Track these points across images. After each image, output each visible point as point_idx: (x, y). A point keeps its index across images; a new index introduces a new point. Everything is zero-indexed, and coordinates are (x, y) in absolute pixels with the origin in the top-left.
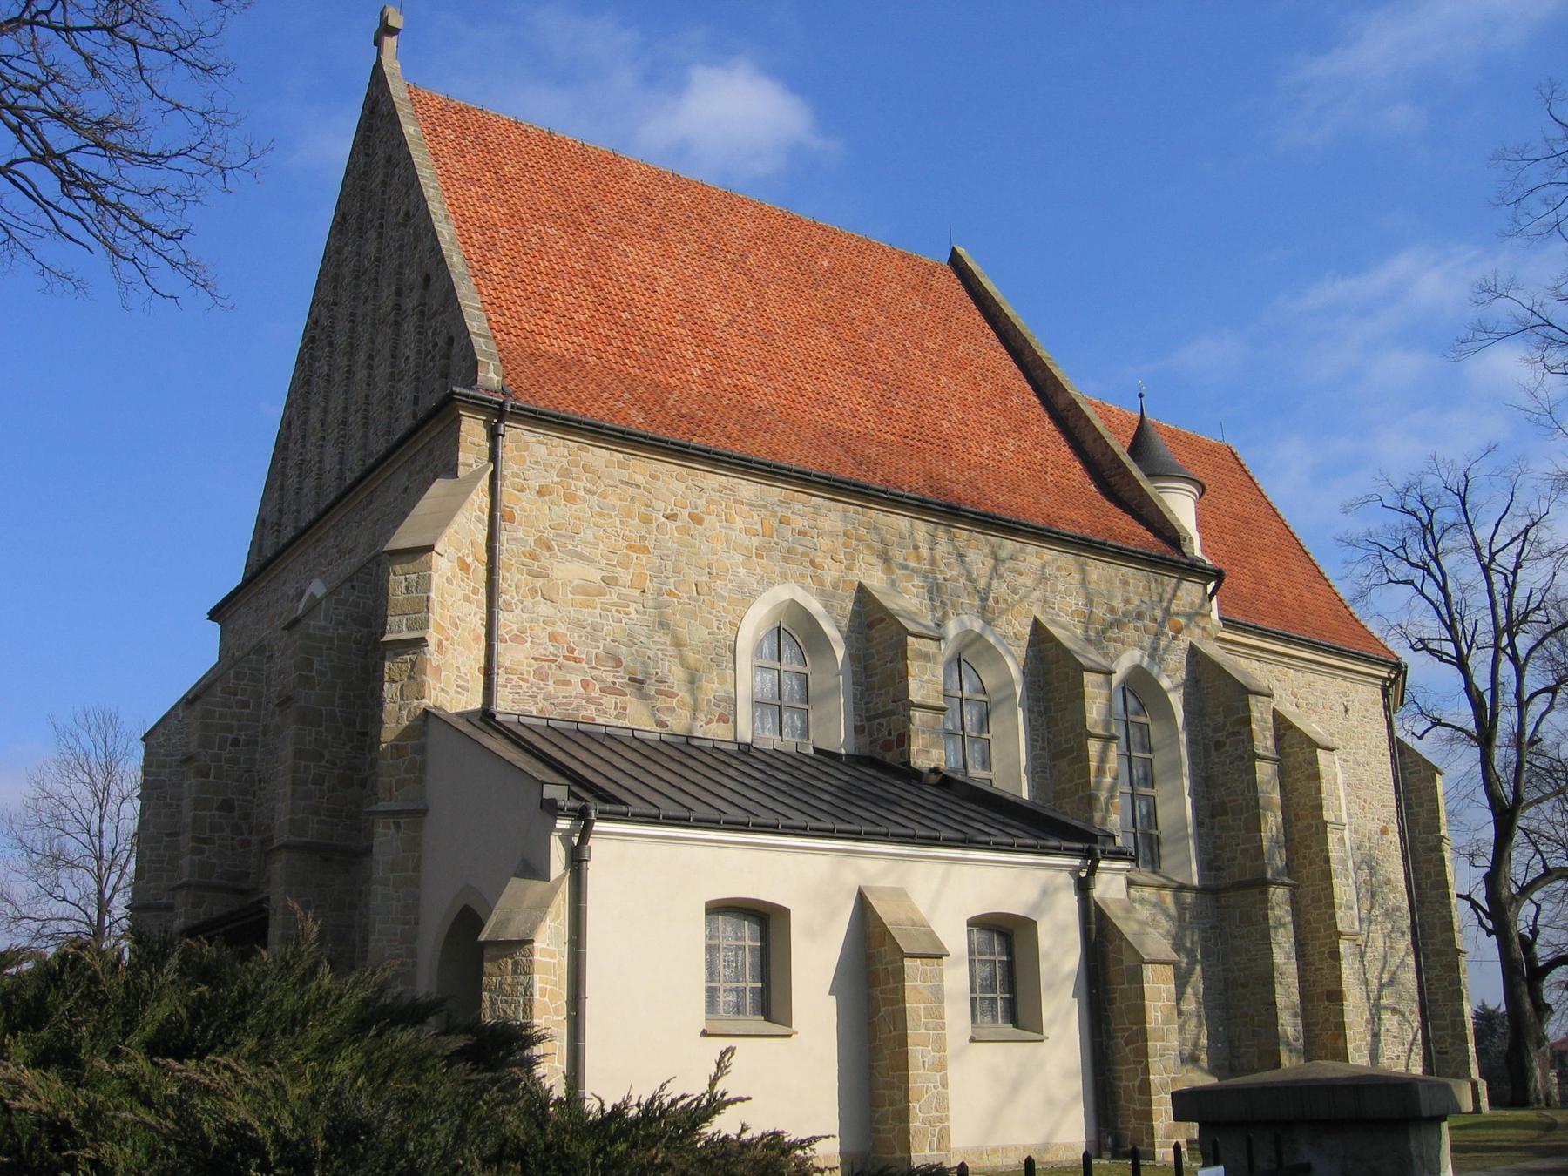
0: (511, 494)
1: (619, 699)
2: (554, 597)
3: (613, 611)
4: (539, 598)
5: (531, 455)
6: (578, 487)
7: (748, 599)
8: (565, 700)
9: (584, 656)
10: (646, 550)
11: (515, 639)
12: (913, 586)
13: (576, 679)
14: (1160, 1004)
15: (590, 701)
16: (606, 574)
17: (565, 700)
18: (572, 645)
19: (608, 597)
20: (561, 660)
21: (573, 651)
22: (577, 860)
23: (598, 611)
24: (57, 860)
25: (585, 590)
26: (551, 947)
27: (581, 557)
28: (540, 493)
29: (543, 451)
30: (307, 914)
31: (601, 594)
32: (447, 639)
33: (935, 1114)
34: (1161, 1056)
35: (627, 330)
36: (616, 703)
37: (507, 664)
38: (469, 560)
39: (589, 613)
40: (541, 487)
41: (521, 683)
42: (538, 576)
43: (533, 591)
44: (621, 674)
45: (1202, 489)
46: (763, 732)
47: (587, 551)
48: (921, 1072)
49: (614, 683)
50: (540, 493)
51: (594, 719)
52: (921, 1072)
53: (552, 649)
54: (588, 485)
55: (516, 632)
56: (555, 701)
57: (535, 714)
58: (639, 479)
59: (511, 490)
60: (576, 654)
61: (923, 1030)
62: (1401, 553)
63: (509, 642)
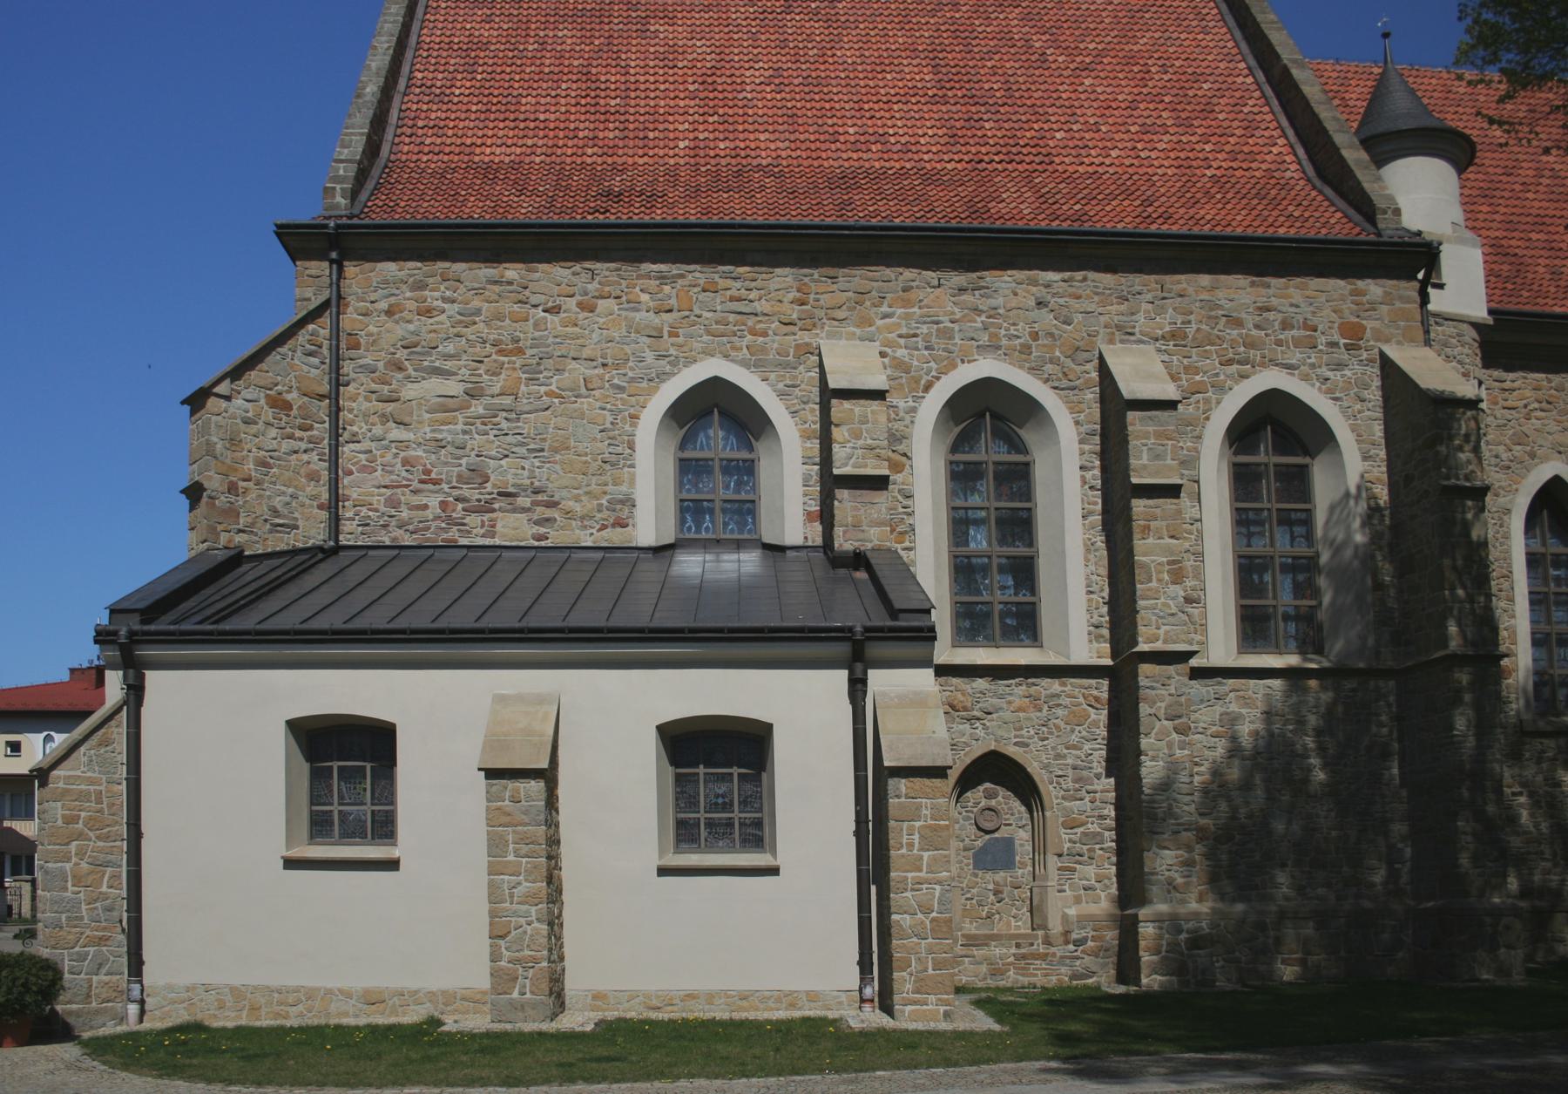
0: (354, 320)
2: (407, 419)
3: (478, 425)
4: (391, 424)
7: (662, 377)
8: (421, 525)
9: (443, 477)
10: (520, 351)
12: (900, 336)
13: (434, 502)
14: (917, 824)
15: (452, 522)
16: (470, 386)
17: (421, 525)
18: (429, 466)
19: (473, 409)
20: (415, 484)
22: (136, 692)
25: (446, 407)
26: (89, 774)
28: (389, 313)
32: (248, 480)
33: (527, 952)
34: (912, 890)
36: (482, 521)
38: (291, 397)
39: (448, 431)
40: (390, 306)
41: (371, 513)
44: (489, 489)
47: (448, 365)
48: (508, 904)
49: (479, 500)
50: (389, 313)
51: (456, 541)
52: (508, 904)
53: (404, 474)
54: (448, 293)
55: (364, 462)
56: (411, 528)
57: (388, 543)
59: (355, 316)
60: (433, 476)
61: (511, 858)
63: (356, 474)
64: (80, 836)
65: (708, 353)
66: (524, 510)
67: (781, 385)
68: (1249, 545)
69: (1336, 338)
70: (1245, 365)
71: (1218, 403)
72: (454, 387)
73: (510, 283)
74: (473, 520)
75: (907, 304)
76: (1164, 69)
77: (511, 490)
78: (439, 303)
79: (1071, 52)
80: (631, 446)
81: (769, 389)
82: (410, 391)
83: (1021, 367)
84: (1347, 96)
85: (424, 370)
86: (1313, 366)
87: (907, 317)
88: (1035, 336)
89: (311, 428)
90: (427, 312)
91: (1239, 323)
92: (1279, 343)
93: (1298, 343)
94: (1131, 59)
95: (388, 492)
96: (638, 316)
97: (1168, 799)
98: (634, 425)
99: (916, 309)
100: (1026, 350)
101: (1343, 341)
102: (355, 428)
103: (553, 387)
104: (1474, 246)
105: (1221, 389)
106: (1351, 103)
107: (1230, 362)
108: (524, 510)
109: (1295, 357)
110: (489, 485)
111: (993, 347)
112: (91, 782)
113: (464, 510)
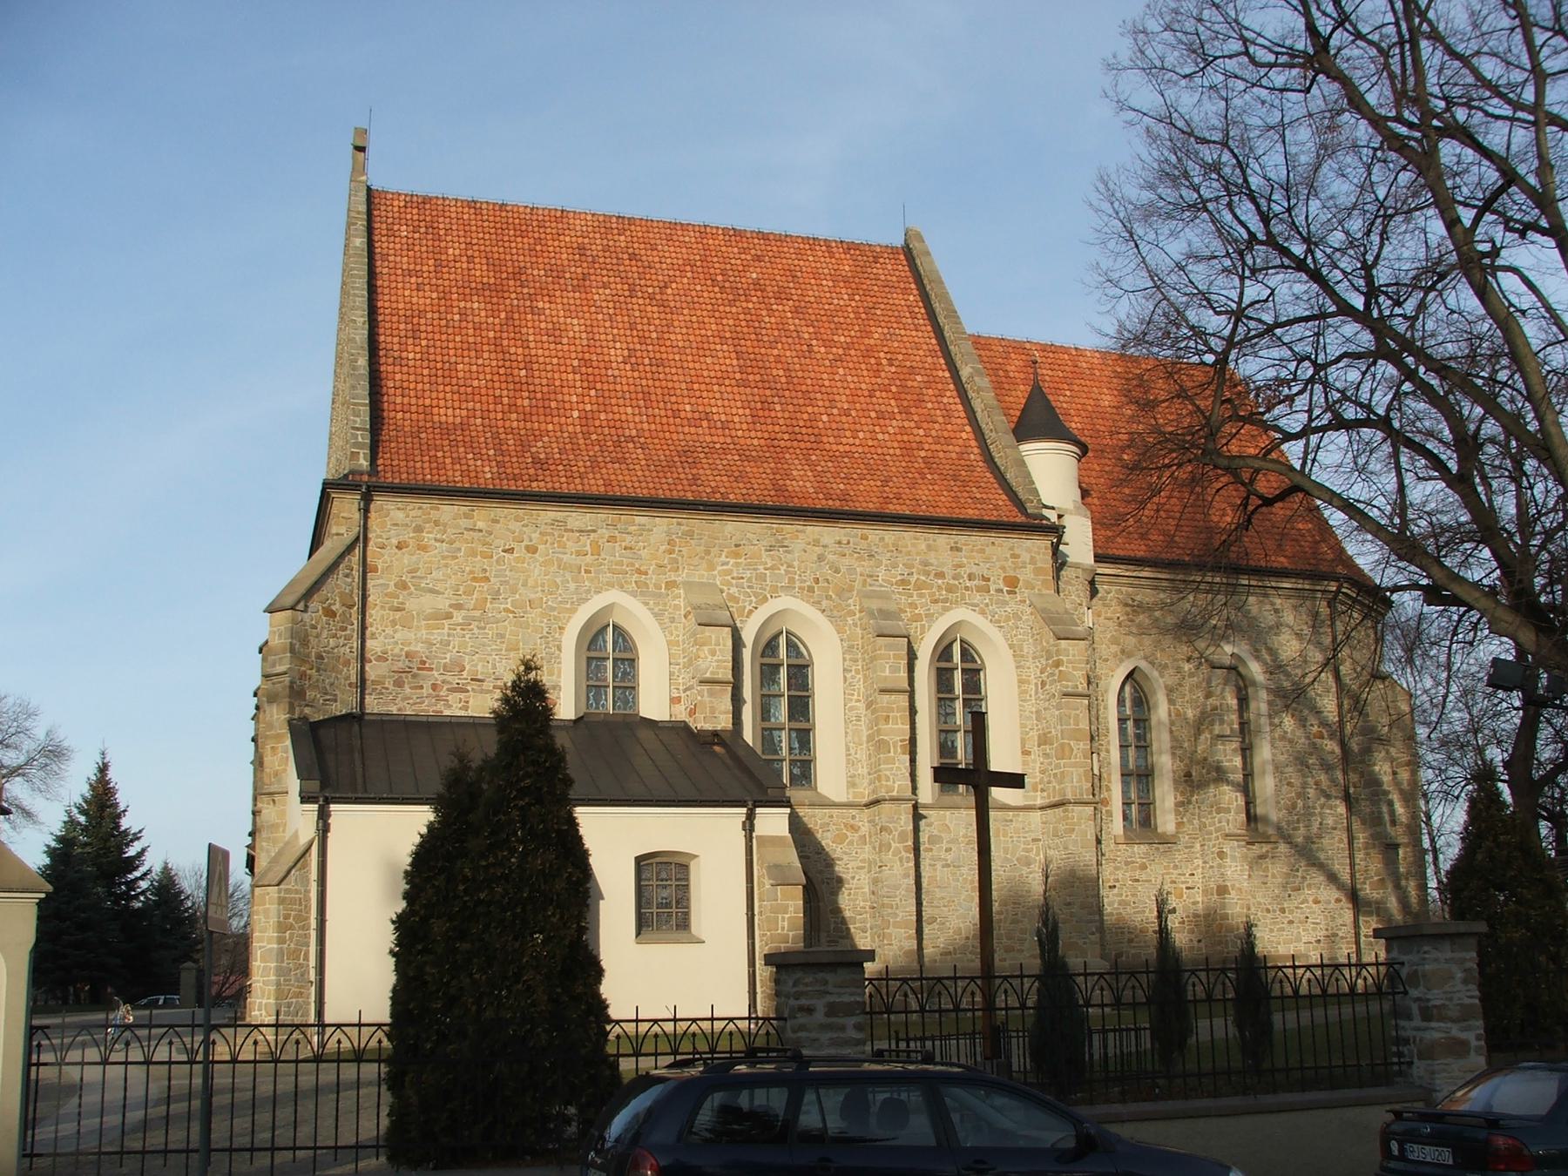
1: (462, 696)
5: (391, 519)
6: (428, 537)
11: (379, 659)
21: (424, 663)
23: (446, 631)
24: (1122, 517)
27: (432, 591)
28: (399, 547)
29: (401, 515)
30: (137, 879)
31: (449, 616)
35: (519, 386)
37: (373, 678)
42: (398, 610)
43: (394, 623)
45: (1084, 449)
46: (597, 708)
50: (399, 547)
54: (439, 536)
58: (480, 525)
62: (1255, 501)
64: (291, 927)
65: (611, 585)
66: (489, 692)
67: (656, 610)
68: (946, 723)
70: (947, 605)
71: (930, 627)
72: (443, 603)
73: (481, 531)
75: (737, 555)
76: (891, 362)
77: (479, 677)
79: (829, 344)
81: (648, 613)
82: (412, 605)
83: (808, 602)
84: (1008, 368)
85: (423, 590)
86: (987, 605)
88: (817, 581)
89: (346, 629)
90: (424, 548)
91: (940, 575)
92: (967, 588)
93: (979, 589)
94: (868, 352)
96: (565, 557)
97: (1104, 1031)
98: (561, 634)
99: (742, 560)
100: (811, 590)
101: (1005, 589)
103: (509, 606)
104: (1085, 516)
105: (930, 617)
106: (1011, 374)
107: (936, 601)
108: (489, 692)
109: (977, 598)
110: (465, 673)
111: (788, 589)
112: (297, 892)
113: (448, 690)
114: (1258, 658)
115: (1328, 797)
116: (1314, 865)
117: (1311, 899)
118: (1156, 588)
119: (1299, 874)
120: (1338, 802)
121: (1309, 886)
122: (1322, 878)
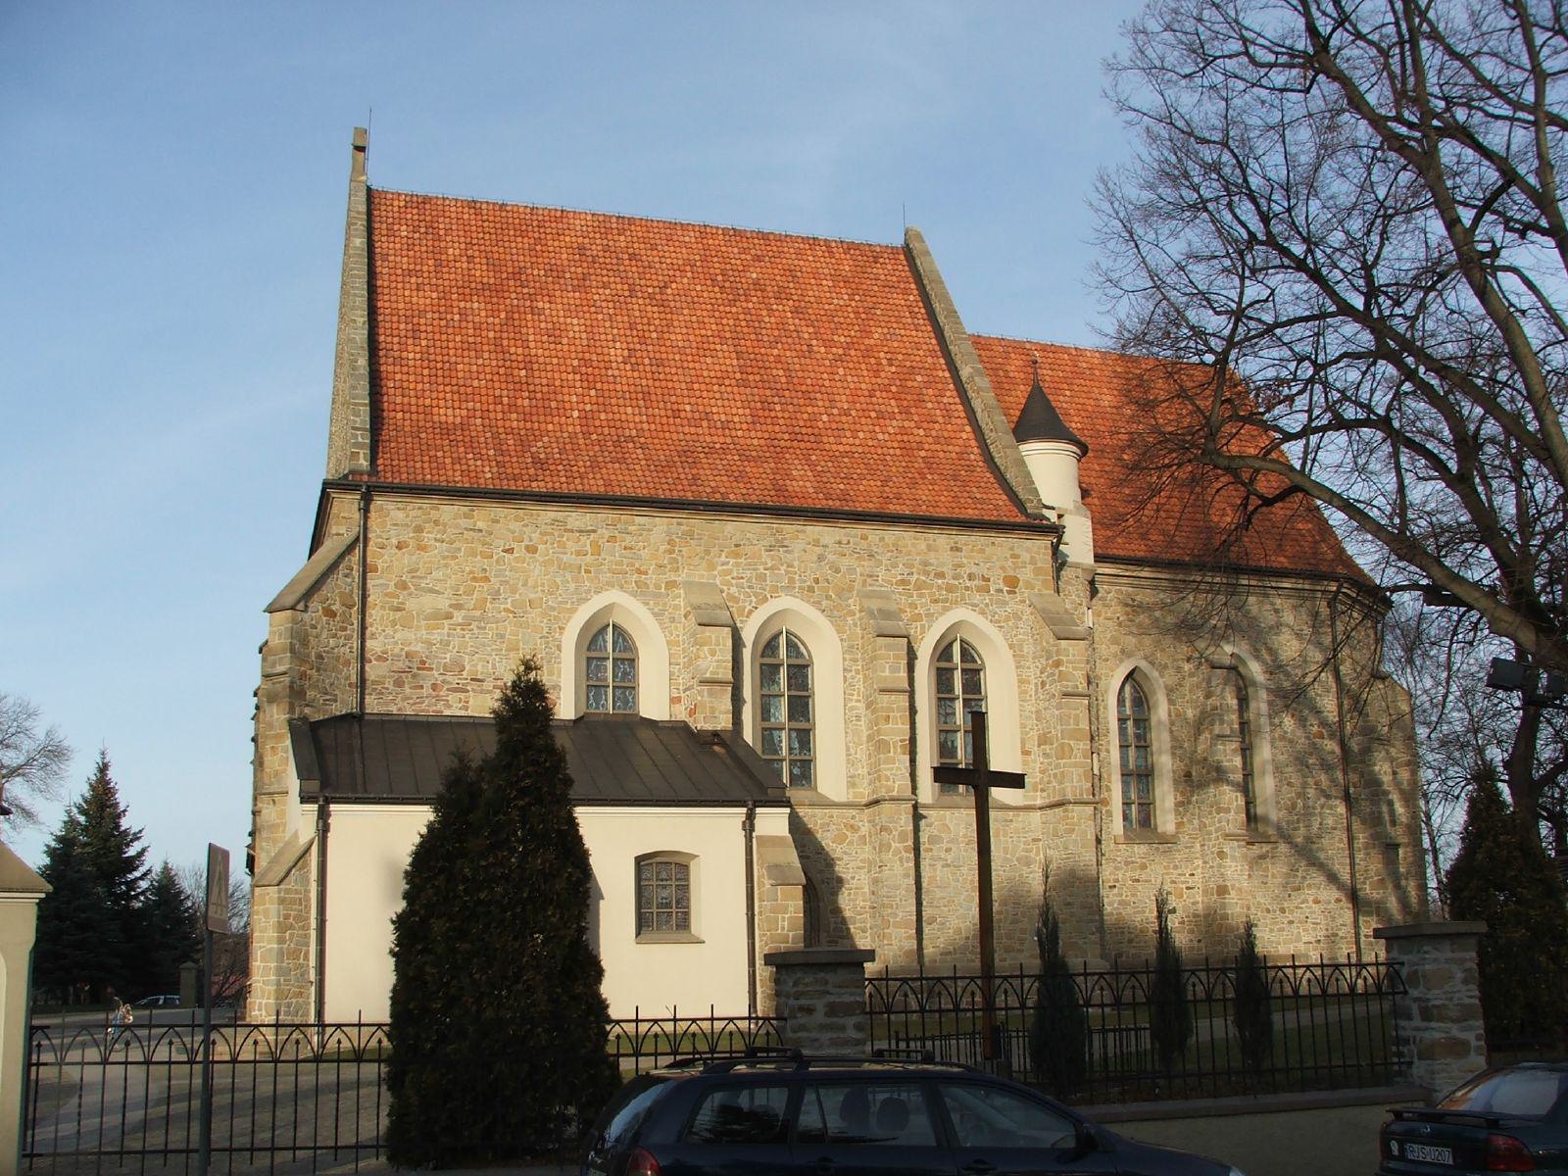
10: (487, 579)
28: (399, 547)
69: (1002, 586)
73: (480, 531)
74: (452, 698)
78: (433, 542)
80: (559, 648)
83: (808, 602)
87: (737, 565)
95: (396, 675)
101: (1006, 589)
102: (373, 629)
114: (1257, 658)
115: (1328, 797)
116: (1314, 865)
117: (1311, 899)
118: (1155, 588)
119: (1299, 874)
120: (1338, 802)
121: (1309, 886)
122: (1322, 878)
